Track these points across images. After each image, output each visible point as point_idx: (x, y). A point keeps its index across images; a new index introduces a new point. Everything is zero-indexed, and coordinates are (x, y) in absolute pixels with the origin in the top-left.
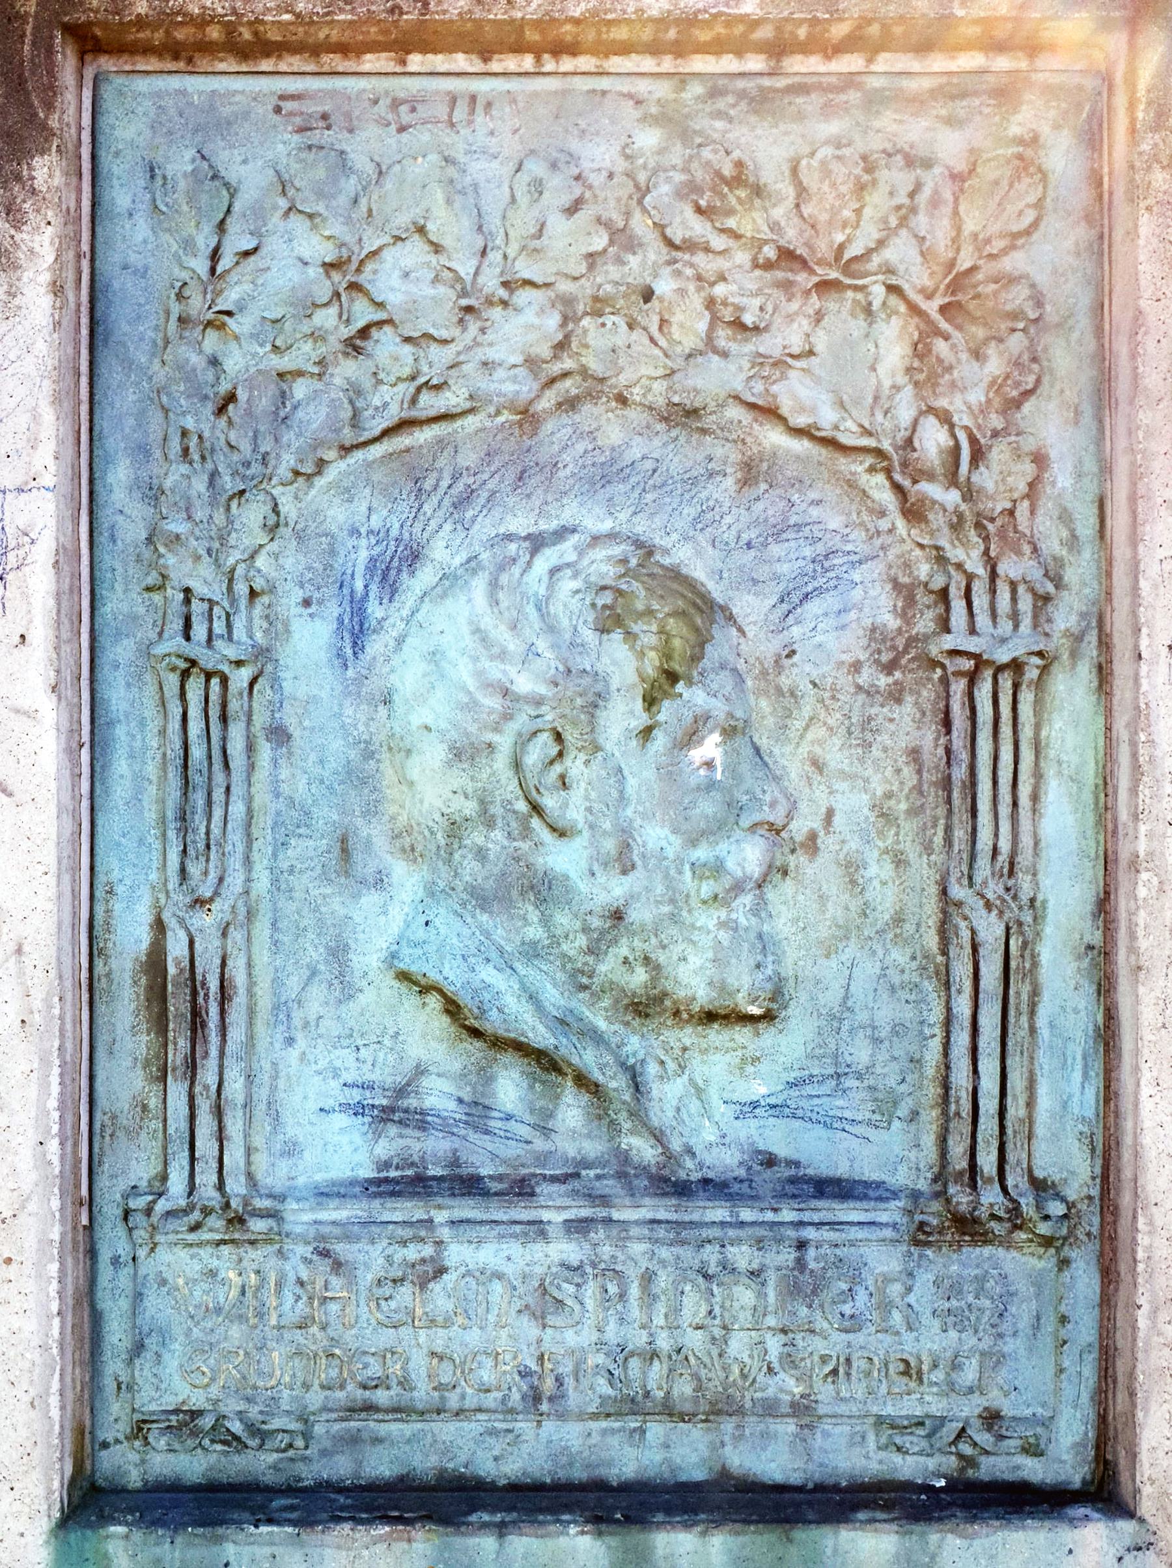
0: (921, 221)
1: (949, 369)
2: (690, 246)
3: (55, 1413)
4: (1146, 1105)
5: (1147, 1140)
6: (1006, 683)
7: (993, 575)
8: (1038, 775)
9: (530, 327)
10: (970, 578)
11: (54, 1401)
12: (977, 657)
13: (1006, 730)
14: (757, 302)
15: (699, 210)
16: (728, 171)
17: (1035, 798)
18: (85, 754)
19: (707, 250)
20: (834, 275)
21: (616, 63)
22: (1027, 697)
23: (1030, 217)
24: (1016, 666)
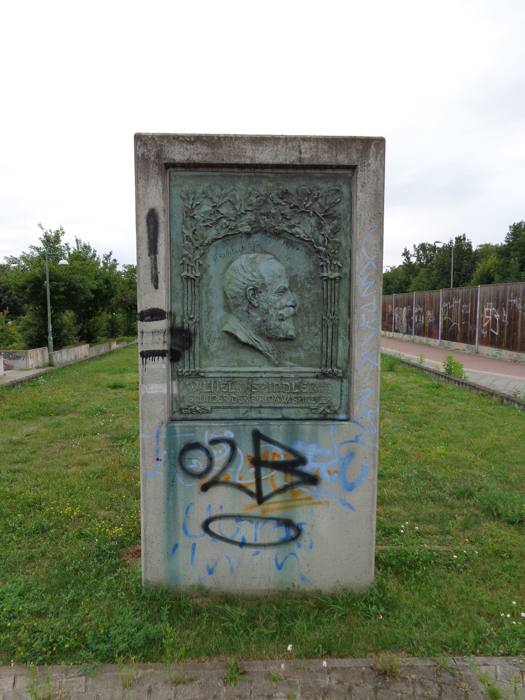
0: (320, 200)
1: (324, 227)
2: (278, 204)
3: (166, 406)
4: (356, 354)
5: (356, 360)
6: (333, 282)
7: (331, 263)
8: (339, 297)
9: (249, 218)
10: (327, 263)
11: (166, 403)
12: (328, 277)
13: (333, 290)
14: (289, 214)
15: (279, 198)
16: (285, 191)
17: (338, 302)
18: (170, 293)
19: (281, 205)
20: (304, 210)
21: (265, 171)
22: (337, 285)
23: (339, 200)
24: (335, 279)
